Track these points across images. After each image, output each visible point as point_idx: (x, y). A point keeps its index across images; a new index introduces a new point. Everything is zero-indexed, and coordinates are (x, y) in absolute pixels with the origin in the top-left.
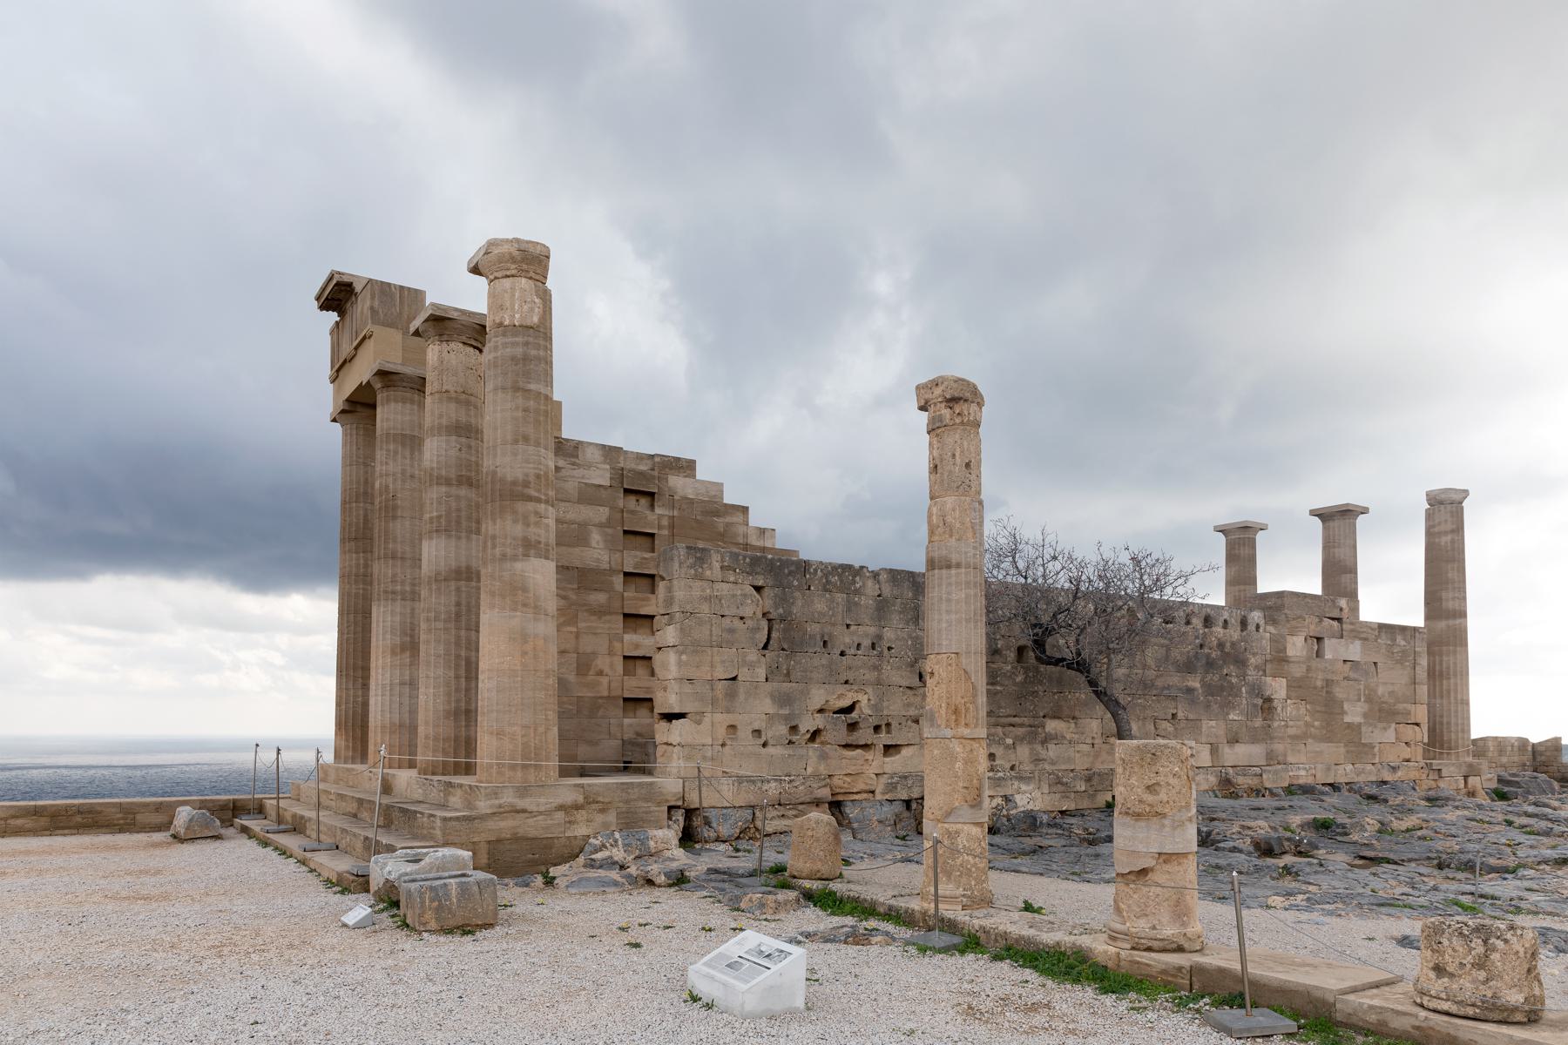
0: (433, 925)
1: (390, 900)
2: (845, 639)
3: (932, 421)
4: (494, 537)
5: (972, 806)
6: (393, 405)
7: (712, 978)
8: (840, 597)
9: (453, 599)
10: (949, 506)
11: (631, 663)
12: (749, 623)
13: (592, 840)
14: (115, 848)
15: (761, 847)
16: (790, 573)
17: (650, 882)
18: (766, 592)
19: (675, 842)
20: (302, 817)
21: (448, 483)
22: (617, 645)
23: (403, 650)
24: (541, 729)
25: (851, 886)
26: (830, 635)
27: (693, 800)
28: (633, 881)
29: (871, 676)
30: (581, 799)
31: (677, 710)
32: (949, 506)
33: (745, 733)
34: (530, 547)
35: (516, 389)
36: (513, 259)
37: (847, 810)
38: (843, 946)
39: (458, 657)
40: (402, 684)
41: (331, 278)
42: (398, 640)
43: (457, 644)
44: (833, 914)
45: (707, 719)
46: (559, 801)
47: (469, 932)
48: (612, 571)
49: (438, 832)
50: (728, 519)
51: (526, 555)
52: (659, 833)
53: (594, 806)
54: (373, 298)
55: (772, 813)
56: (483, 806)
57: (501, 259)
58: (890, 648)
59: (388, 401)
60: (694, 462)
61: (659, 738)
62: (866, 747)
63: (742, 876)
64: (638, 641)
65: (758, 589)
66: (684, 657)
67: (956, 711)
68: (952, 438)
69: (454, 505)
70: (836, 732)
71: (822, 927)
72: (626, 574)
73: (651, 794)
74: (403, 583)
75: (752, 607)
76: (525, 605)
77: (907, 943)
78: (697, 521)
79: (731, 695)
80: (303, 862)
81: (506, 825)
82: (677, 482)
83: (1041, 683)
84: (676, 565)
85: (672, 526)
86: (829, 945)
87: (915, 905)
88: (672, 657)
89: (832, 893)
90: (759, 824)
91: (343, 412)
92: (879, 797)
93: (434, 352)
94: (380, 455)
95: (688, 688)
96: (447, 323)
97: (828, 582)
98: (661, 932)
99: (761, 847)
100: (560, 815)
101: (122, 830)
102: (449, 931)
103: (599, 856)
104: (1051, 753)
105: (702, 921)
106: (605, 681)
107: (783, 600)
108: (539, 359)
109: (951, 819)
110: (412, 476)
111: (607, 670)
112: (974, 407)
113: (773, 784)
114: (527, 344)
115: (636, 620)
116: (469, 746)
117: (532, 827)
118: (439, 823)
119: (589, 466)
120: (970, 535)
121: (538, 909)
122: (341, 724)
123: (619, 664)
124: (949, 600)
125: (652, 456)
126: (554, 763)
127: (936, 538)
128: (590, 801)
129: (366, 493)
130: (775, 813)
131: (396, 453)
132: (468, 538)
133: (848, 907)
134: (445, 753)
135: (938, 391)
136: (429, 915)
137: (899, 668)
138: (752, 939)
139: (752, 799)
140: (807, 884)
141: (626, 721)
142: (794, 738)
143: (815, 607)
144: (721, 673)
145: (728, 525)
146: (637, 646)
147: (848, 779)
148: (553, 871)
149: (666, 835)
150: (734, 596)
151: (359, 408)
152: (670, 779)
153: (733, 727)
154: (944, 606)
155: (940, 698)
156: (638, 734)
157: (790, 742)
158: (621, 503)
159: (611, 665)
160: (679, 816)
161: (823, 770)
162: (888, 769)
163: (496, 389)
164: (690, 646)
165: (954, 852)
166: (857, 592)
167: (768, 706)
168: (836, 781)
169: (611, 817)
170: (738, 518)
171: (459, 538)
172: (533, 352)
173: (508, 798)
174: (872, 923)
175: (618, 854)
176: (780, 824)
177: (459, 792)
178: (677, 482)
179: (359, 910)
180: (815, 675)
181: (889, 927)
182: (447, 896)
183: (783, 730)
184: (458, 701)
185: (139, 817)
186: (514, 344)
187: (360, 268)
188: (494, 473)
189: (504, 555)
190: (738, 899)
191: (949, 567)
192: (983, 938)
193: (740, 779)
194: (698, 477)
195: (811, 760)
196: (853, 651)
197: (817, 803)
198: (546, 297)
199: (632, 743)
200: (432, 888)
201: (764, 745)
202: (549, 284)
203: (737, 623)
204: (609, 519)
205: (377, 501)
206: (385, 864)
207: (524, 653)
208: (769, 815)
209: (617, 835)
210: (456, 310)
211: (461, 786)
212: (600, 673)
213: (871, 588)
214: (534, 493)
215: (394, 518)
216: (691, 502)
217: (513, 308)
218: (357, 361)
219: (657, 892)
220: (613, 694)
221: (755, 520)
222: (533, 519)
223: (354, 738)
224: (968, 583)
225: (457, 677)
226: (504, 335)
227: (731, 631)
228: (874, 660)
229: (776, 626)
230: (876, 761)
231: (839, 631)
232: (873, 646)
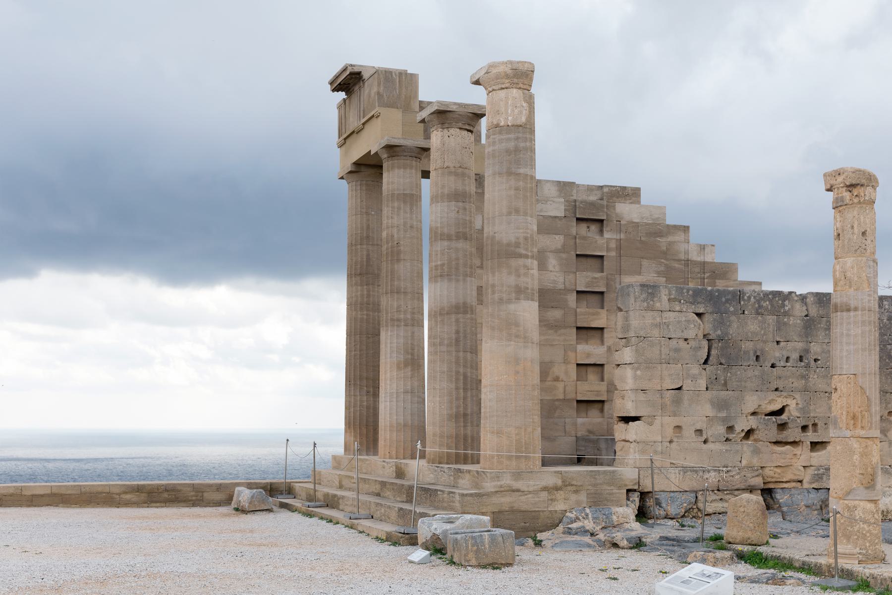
0: (474, 562)
1: (437, 548)
2: (775, 353)
3: (836, 200)
4: (493, 286)
5: (867, 488)
6: (396, 171)
7: (672, 589)
8: (771, 319)
9: (454, 328)
10: (849, 264)
11: (583, 369)
12: (692, 343)
13: (568, 514)
14: (199, 516)
15: (703, 524)
16: (727, 301)
17: (615, 545)
18: (706, 318)
19: (633, 517)
20: (335, 496)
21: (449, 238)
22: (571, 355)
23: (406, 366)
24: (530, 430)
25: (773, 549)
26: (762, 350)
27: (647, 486)
28: (602, 545)
29: (799, 384)
30: (560, 483)
31: (633, 414)
32: (849, 264)
33: (688, 432)
34: (520, 292)
35: (509, 173)
36: (507, 76)
37: (778, 496)
38: (764, 585)
39: (457, 373)
40: (406, 392)
41: (345, 70)
42: (402, 358)
43: (457, 362)
44: (759, 568)
45: (658, 421)
46: (544, 483)
47: (497, 568)
48: (567, 290)
49: (457, 505)
50: (670, 238)
51: (518, 299)
52: (620, 510)
53: (569, 488)
54: (379, 85)
55: (711, 497)
56: (489, 486)
57: (498, 77)
58: (816, 360)
59: (393, 168)
60: (639, 189)
61: (618, 436)
62: (794, 443)
63: (688, 541)
64: (591, 351)
65: (699, 315)
66: (639, 372)
67: (854, 418)
68: (851, 214)
69: (454, 256)
70: (768, 431)
71: (750, 574)
72: (578, 292)
73: (613, 479)
74: (405, 312)
75: (695, 330)
76: (517, 336)
77: (814, 584)
78: (641, 242)
79: (677, 402)
80: (352, 527)
81: (506, 501)
84: (632, 300)
85: (619, 248)
86: (754, 585)
87: (823, 561)
88: (629, 372)
89: (759, 554)
90: (701, 505)
91: (350, 172)
92: (806, 485)
93: (437, 138)
94: (386, 211)
95: (642, 397)
96: (448, 115)
97: (760, 307)
98: (630, 572)
99: (703, 524)
100: (544, 494)
101: (194, 505)
102: (484, 567)
103: (574, 526)
105: (660, 567)
106: (560, 385)
107: (721, 323)
108: (526, 149)
109: (850, 497)
110: (412, 227)
111: (562, 376)
112: (869, 189)
113: (713, 474)
114: (517, 139)
115: (585, 331)
116: (473, 441)
117: (525, 503)
118: (457, 497)
119: (546, 201)
120: (865, 285)
121: (538, 558)
122: (350, 423)
123: (573, 368)
124: (848, 335)
125: (601, 187)
126: (539, 455)
127: (839, 288)
128: (566, 484)
129: (368, 237)
130: (714, 497)
131: (399, 208)
132: (464, 280)
133: (771, 563)
134: (441, 446)
135: (840, 179)
136: (471, 555)
138: (696, 568)
139: (695, 485)
140: (740, 548)
141: (580, 421)
142: (731, 436)
143: (748, 328)
145: (670, 244)
146: (589, 355)
147: (778, 470)
148: (540, 536)
149: (627, 512)
150: (679, 322)
151: (363, 169)
152: (629, 467)
153: (678, 428)
154: (844, 340)
155: (842, 408)
156: (590, 432)
157: (727, 440)
158: (574, 231)
159: (566, 373)
160: (636, 497)
161: (756, 462)
162: (814, 462)
163: (494, 174)
164: (644, 364)
165: (852, 520)
166: (786, 314)
167: (708, 410)
168: (768, 472)
169: (583, 497)
170: (679, 237)
171: (457, 281)
172: (522, 145)
173: (507, 481)
174: (790, 573)
175: (589, 525)
176: (719, 506)
177: (467, 476)
178: (625, 210)
179: (419, 554)
181: (803, 576)
182: (483, 542)
183: (721, 429)
184: (458, 407)
185: (205, 494)
186: (509, 140)
187: (368, 59)
188: (493, 237)
189: (501, 299)
190: (685, 555)
191: (849, 310)
192: (872, 582)
193: (685, 469)
194: (642, 203)
195: (746, 454)
196: (782, 363)
197: (751, 490)
198: (530, 100)
199: (586, 440)
200: (473, 538)
201: (705, 442)
202: (532, 91)
203: (682, 344)
204: (564, 246)
205: (384, 248)
206: (431, 524)
207: (517, 372)
208: (709, 499)
209: (588, 510)
210: (455, 104)
211: (469, 471)
212: (557, 379)
213: (799, 310)
214: (523, 252)
215: (398, 260)
216: (636, 225)
217: (507, 113)
218: (364, 133)
219: (622, 552)
220: (568, 397)
221: (696, 237)
222: (522, 271)
223: (361, 434)
224: (870, 322)
225: (457, 389)
226: (500, 133)
227: (677, 350)
228: (802, 371)
229: (715, 345)
230: (803, 455)
231: (770, 347)
232: (801, 359)
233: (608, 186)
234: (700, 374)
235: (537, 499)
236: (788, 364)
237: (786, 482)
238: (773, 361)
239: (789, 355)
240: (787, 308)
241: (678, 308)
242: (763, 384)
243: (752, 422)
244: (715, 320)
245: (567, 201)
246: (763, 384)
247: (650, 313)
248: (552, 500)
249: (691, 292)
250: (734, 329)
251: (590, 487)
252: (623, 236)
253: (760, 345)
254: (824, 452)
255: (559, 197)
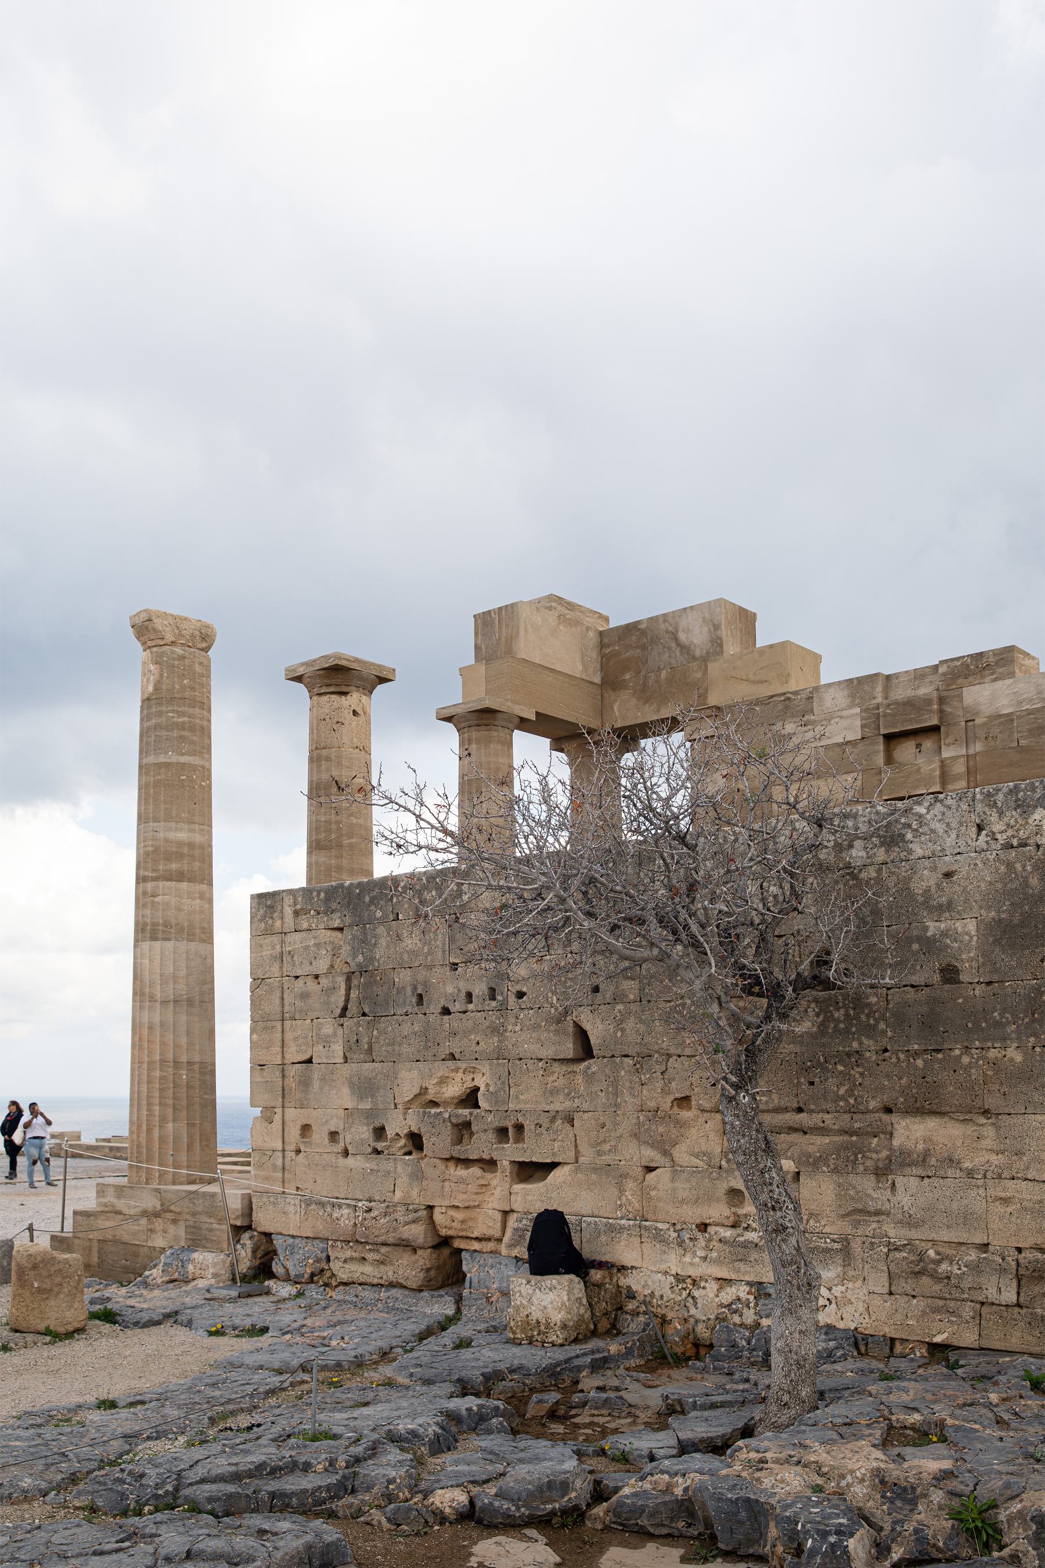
12: (323, 981)
26: (425, 983)
33: (319, 1136)
53: (168, 1215)
58: (520, 995)
79: (305, 1083)
82: (986, 697)
83: (870, 1031)
104: (903, 1199)
107: (364, 943)
113: (345, 1211)
137: (536, 1027)
139: (321, 1228)
144: (294, 1054)
147: (459, 1215)
150: (306, 948)
161: (417, 1197)
167: (345, 1098)
180: (405, 1049)
183: (364, 1132)
201: (346, 1153)
203: (312, 986)
210: (302, 664)
216: (1009, 718)
227: (304, 996)
228: (493, 1017)
232: (492, 994)
233: (946, 661)
234: (335, 1035)
235: (136, 1227)
236: (471, 1007)
237: (478, 1239)
238: (443, 1002)
239: (470, 988)
240: (465, 898)
241: (305, 926)
242: (427, 1048)
243: (413, 1122)
244: (354, 937)
245: (866, 710)
246: (427, 1048)
247: (269, 939)
248: (151, 1230)
249: (322, 895)
250: (382, 952)
251: (188, 1217)
252: (978, 747)
253: (422, 975)
254: (541, 1184)
255: (851, 706)
